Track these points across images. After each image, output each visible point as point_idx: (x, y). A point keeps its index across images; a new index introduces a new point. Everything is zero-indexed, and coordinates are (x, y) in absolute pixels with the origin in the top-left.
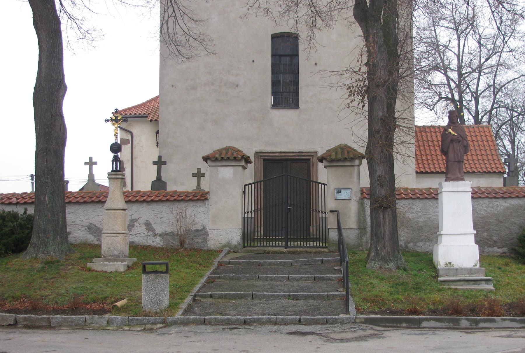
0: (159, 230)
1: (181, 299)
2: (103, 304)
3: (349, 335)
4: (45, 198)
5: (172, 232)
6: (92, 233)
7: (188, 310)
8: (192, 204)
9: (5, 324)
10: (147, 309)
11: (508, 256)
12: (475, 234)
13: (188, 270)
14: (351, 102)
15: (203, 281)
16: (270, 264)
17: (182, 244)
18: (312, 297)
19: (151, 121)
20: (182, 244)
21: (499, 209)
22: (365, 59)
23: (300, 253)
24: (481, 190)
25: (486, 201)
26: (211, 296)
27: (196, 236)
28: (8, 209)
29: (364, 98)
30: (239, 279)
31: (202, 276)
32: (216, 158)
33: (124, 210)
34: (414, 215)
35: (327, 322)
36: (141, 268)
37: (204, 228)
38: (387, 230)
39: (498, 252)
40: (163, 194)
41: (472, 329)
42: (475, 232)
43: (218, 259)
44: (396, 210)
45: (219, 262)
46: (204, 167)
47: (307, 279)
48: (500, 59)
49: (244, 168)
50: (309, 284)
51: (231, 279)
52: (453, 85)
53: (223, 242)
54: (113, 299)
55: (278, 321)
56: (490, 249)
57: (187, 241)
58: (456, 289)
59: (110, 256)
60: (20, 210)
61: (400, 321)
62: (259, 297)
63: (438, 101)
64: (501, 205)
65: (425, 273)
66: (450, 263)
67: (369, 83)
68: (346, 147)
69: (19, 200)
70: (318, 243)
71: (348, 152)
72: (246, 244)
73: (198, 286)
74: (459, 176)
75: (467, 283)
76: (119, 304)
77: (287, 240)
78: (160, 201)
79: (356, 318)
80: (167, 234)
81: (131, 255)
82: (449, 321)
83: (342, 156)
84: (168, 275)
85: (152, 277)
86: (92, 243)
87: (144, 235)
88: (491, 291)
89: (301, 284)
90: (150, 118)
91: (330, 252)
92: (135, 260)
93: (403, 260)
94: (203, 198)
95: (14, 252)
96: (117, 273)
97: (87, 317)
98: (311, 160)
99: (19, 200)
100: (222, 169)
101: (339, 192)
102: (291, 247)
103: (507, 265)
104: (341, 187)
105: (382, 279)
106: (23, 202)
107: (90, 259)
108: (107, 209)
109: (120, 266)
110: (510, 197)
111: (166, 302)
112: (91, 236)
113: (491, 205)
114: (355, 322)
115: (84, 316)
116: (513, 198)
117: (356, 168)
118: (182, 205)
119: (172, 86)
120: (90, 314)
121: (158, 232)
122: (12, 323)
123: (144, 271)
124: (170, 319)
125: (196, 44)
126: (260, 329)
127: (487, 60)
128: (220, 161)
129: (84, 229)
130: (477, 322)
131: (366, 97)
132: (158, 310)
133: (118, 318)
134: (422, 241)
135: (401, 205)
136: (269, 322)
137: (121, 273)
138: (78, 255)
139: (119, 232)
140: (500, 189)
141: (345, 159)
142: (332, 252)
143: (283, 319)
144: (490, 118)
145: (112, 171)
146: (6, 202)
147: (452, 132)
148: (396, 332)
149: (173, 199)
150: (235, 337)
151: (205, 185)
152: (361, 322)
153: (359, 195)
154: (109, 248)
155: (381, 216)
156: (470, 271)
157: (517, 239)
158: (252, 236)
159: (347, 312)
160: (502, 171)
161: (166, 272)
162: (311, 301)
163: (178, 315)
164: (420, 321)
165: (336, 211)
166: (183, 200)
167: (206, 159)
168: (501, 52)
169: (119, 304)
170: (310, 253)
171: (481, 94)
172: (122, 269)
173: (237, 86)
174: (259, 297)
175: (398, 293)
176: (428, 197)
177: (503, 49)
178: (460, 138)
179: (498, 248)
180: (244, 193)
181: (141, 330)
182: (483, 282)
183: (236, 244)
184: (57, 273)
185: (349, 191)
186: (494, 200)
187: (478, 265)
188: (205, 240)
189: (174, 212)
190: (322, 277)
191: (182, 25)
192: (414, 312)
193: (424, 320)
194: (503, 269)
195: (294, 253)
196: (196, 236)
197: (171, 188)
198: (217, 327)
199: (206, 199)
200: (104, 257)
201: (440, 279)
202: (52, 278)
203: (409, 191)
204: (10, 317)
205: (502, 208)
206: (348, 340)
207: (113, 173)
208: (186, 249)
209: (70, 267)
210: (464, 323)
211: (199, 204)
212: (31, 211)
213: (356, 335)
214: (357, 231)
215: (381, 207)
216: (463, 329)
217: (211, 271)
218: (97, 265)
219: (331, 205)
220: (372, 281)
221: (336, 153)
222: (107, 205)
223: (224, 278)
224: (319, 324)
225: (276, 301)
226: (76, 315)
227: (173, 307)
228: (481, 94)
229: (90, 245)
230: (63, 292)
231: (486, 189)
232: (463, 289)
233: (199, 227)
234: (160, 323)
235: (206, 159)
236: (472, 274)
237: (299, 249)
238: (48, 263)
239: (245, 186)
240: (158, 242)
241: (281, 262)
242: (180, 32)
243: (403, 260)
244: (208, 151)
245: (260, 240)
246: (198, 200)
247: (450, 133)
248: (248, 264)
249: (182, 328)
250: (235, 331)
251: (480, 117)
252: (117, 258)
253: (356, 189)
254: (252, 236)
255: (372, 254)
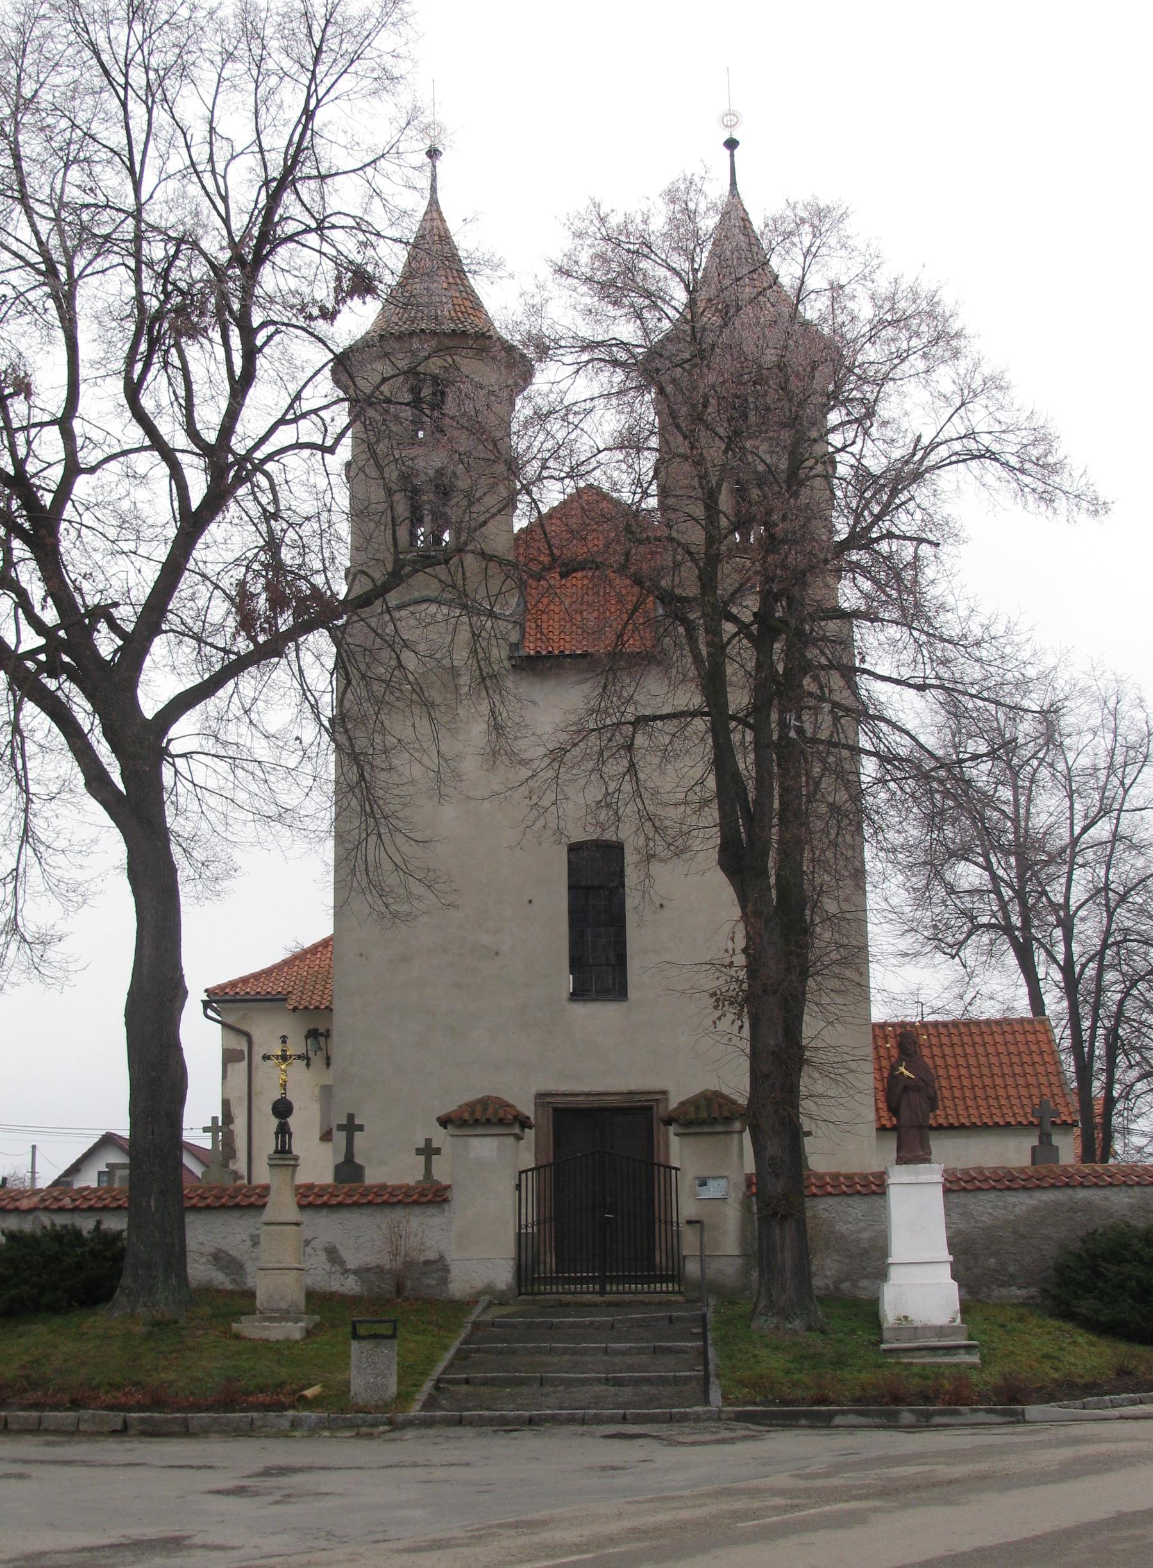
0: (352, 1262)
1: (415, 1385)
2: (278, 1394)
3: (708, 1437)
4: (148, 1202)
5: (378, 1266)
6: (220, 1269)
7: (430, 1403)
8: (417, 1210)
9: (106, 1429)
10: (360, 1400)
11: (1037, 1305)
12: (951, 1263)
13: (420, 1338)
14: (719, 1018)
15: (448, 1355)
16: (573, 1325)
17: (399, 1289)
18: (648, 1381)
19: (295, 1009)
20: (399, 1289)
21: (1017, 1210)
22: (741, 943)
23: (629, 1304)
24: (983, 1174)
25: (992, 1196)
26: (467, 1381)
27: (425, 1274)
28: (61, 1220)
29: (741, 1011)
30: (514, 1352)
31: (445, 1348)
32: (465, 1121)
33: (297, 1224)
34: (849, 1226)
35: (671, 1419)
36: (349, 1329)
37: (442, 1258)
38: (787, 1257)
39: (1017, 1297)
40: (360, 1190)
41: (920, 1427)
42: (951, 1258)
43: (472, 1318)
44: (804, 1220)
45: (474, 1323)
46: (441, 1137)
47: (640, 1351)
48: (1117, 827)
49: (519, 1138)
50: (644, 1359)
51: (500, 1352)
52: (1007, 893)
53: (479, 1284)
54: (294, 1386)
55: (587, 1418)
56: (1004, 1291)
57: (409, 1284)
58: (911, 1364)
59: (273, 1311)
60: (86, 1225)
61: (797, 1415)
62: (552, 1382)
63: (970, 934)
64: (1021, 1204)
65: (860, 1336)
66: (906, 1318)
67: (750, 986)
68: (717, 1094)
69: (77, 1203)
70: (670, 1285)
71: (720, 1106)
72: (523, 1290)
73: (441, 1365)
74: (921, 1153)
75: (931, 1353)
76: (309, 1393)
77: (603, 1280)
78: (356, 1205)
79: (720, 1411)
80: (368, 1270)
81: (309, 1310)
82: (881, 1414)
83: (709, 1115)
84: (396, 1342)
85: (368, 1345)
86: (220, 1287)
87: (322, 1272)
88: (973, 1366)
89: (628, 1359)
90: (292, 1003)
91: (688, 1301)
92: (317, 1318)
93: (820, 1313)
94: (440, 1199)
95: (83, 1304)
96: (289, 1343)
97: (255, 1415)
98: (655, 1109)
99: (77, 1203)
100: (475, 1142)
101: (703, 1183)
102: (612, 1293)
103: (1021, 1319)
104: (707, 1174)
105: (777, 1348)
106: (85, 1206)
107: (236, 1315)
108: (266, 1224)
109: (294, 1331)
110: (1038, 1187)
111: (393, 1389)
112: (219, 1273)
113: (1001, 1204)
114: (720, 1419)
115: (249, 1414)
116: (1045, 1188)
117: (736, 1137)
118: (399, 1213)
119: (361, 955)
120: (258, 1411)
121: (351, 1265)
122: (119, 1428)
123: (355, 1336)
124: (401, 1417)
125: (418, 889)
126: (556, 1431)
127: (1085, 829)
128: (470, 1125)
129: (205, 1259)
130: (928, 1415)
131: (746, 1010)
132: (380, 1402)
133: (310, 1416)
134: (867, 1277)
135: (822, 1209)
136: (572, 1420)
137: (297, 1342)
138: (208, 1310)
139: (290, 1266)
140: (1022, 1170)
141: (714, 1121)
142: (692, 1301)
143: (595, 1415)
144: (1101, 970)
145: (276, 1152)
146: (54, 1207)
147: (906, 1073)
148: (788, 1433)
149: (380, 1200)
150: (515, 1442)
151: (442, 1172)
152: (729, 1419)
153: (744, 1188)
154: (271, 1296)
155: (777, 1231)
156: (940, 1331)
157: (1056, 1270)
158: (530, 1272)
159: (707, 1402)
160: (1069, 1121)
161: (393, 1336)
162: (645, 1388)
163: (415, 1410)
164: (831, 1415)
165: (697, 1222)
166: (399, 1202)
167: (444, 1122)
168: (1120, 810)
169: (309, 1393)
170: (649, 1304)
171: (1076, 912)
172: (297, 1335)
173: (497, 954)
174: (552, 1382)
175: (800, 1371)
176: (863, 1190)
177: (1122, 804)
178: (921, 1084)
179: (1019, 1288)
180: (518, 1187)
181: (351, 1437)
182: (962, 1351)
183: (504, 1287)
184: (180, 1342)
185: (723, 1182)
186: (1007, 1193)
187: (958, 1320)
188: (444, 1281)
189: (384, 1226)
190: (667, 1348)
191: (391, 850)
192: (823, 1401)
193: (836, 1413)
194: (1009, 1327)
195: (617, 1305)
196: (425, 1274)
197: (372, 1177)
198: (484, 1429)
199: (446, 1200)
200: (261, 1313)
201: (883, 1346)
202: (171, 1352)
203: (842, 1179)
204: (115, 1416)
205: (1024, 1208)
206: (703, 1443)
207: (277, 1156)
208: (406, 1299)
209: (200, 1332)
210: (907, 1417)
211: (432, 1210)
212: (115, 1224)
213: (718, 1436)
214: (740, 1261)
215: (775, 1214)
216: (905, 1427)
217: (461, 1339)
218: (250, 1328)
219: (687, 1208)
220: (757, 1352)
221: (697, 1108)
222: (269, 1214)
223: (487, 1351)
224: (658, 1422)
225: (584, 1388)
226: (234, 1411)
227: (403, 1398)
228: (1076, 912)
229: (218, 1291)
230: (200, 1374)
231: (995, 1170)
232: (923, 1364)
233: (432, 1256)
234: (384, 1424)
235: (444, 1122)
236: (944, 1336)
237: (628, 1297)
238: (157, 1324)
239: (521, 1173)
240: (350, 1285)
241: (592, 1323)
242: (387, 865)
243: (820, 1313)
244: (451, 1105)
245: (550, 1281)
246: (430, 1202)
247: (902, 1073)
248: (530, 1326)
249: (424, 1431)
250: (515, 1434)
251: (1077, 969)
252: (285, 1316)
253: (737, 1178)
254: (530, 1272)
255: (762, 1305)
